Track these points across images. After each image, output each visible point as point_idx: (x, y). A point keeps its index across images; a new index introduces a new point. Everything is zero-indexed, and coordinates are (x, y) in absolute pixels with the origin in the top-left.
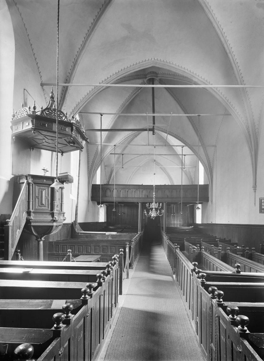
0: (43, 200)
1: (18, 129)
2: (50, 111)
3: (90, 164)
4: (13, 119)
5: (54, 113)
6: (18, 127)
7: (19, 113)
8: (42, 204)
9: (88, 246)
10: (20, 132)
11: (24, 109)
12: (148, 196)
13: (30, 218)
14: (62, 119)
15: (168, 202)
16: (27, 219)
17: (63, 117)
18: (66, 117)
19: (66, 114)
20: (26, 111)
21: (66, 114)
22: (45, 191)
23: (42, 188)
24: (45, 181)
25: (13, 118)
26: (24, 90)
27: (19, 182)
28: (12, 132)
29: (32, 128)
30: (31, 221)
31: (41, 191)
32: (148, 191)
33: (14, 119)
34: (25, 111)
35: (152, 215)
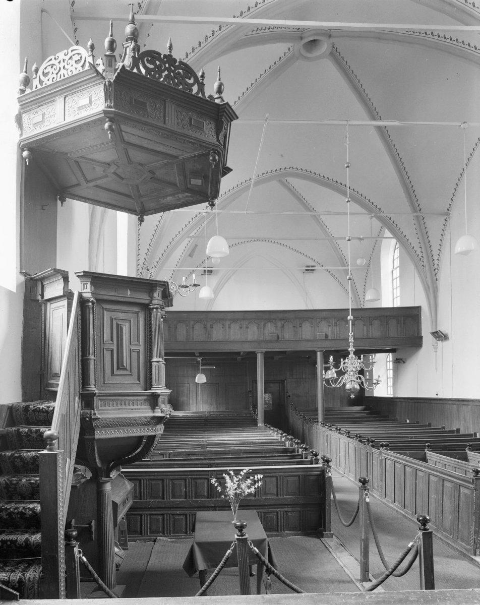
0: (124, 351)
1: (42, 121)
2: (158, 63)
3: (143, 251)
4: (22, 91)
5: (166, 69)
6: (43, 115)
7: (49, 69)
8: (120, 366)
9: (200, 479)
10: (49, 130)
11: (70, 54)
12: (280, 336)
13: (93, 417)
14: (192, 90)
15: (326, 349)
16: (83, 419)
17: (193, 85)
18: (201, 87)
19: (203, 76)
20: (77, 57)
21: (203, 76)
22: (127, 324)
23: (121, 315)
24: (129, 293)
25: (22, 87)
26: (42, 11)
27: (42, 296)
28: (21, 135)
29: (104, 112)
30: (94, 424)
31: (117, 325)
32: (280, 324)
33: (28, 91)
34: (71, 58)
35: (348, 386)
